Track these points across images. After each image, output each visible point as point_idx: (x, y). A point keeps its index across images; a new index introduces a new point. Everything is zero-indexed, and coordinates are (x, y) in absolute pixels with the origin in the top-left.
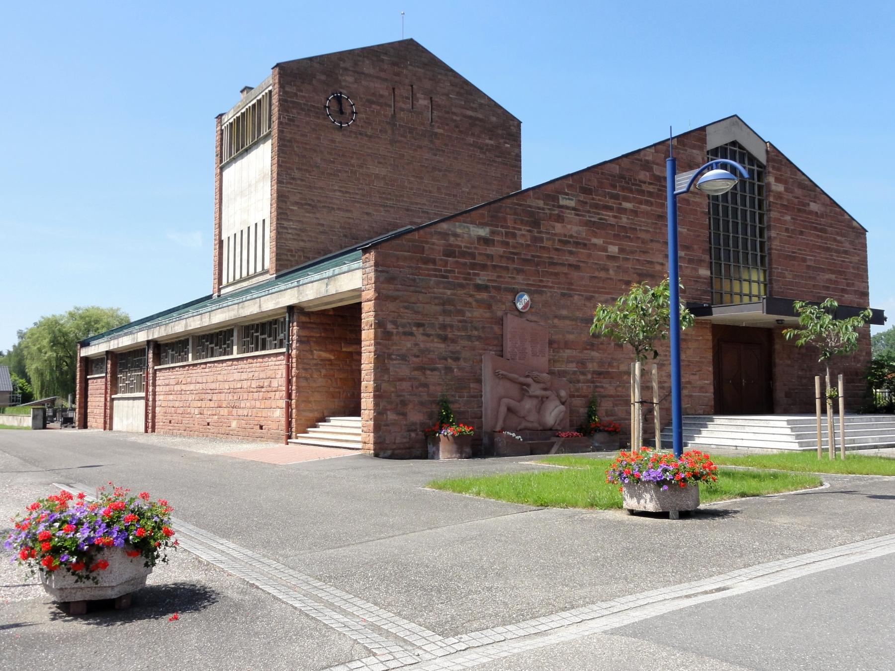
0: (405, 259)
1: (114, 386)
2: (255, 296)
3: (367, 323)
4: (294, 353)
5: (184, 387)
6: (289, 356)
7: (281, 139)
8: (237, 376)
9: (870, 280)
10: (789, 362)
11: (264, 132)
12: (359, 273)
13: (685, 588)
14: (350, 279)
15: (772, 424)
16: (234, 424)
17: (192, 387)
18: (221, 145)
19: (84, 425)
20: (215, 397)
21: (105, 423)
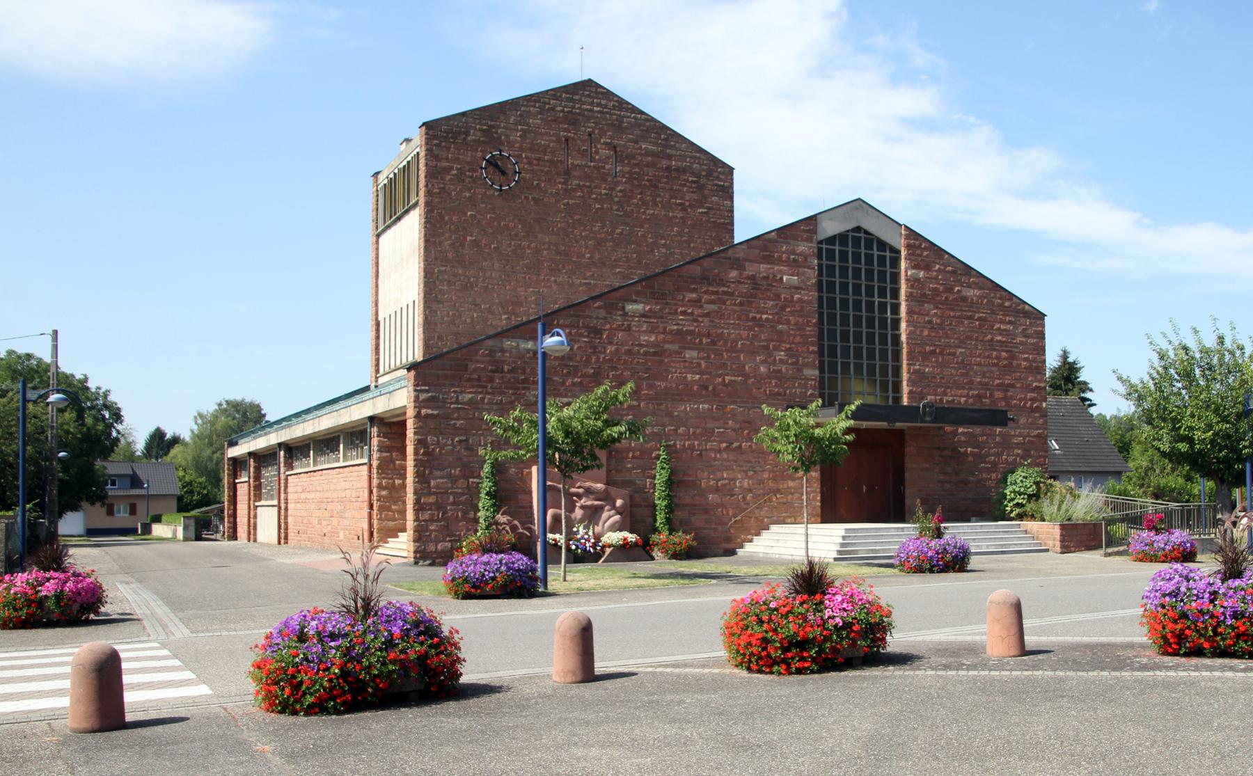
1: (257, 491)
6: (371, 465)
7: (427, 204)
10: (926, 466)
11: (413, 202)
15: (822, 532)
19: (234, 536)
21: (249, 533)
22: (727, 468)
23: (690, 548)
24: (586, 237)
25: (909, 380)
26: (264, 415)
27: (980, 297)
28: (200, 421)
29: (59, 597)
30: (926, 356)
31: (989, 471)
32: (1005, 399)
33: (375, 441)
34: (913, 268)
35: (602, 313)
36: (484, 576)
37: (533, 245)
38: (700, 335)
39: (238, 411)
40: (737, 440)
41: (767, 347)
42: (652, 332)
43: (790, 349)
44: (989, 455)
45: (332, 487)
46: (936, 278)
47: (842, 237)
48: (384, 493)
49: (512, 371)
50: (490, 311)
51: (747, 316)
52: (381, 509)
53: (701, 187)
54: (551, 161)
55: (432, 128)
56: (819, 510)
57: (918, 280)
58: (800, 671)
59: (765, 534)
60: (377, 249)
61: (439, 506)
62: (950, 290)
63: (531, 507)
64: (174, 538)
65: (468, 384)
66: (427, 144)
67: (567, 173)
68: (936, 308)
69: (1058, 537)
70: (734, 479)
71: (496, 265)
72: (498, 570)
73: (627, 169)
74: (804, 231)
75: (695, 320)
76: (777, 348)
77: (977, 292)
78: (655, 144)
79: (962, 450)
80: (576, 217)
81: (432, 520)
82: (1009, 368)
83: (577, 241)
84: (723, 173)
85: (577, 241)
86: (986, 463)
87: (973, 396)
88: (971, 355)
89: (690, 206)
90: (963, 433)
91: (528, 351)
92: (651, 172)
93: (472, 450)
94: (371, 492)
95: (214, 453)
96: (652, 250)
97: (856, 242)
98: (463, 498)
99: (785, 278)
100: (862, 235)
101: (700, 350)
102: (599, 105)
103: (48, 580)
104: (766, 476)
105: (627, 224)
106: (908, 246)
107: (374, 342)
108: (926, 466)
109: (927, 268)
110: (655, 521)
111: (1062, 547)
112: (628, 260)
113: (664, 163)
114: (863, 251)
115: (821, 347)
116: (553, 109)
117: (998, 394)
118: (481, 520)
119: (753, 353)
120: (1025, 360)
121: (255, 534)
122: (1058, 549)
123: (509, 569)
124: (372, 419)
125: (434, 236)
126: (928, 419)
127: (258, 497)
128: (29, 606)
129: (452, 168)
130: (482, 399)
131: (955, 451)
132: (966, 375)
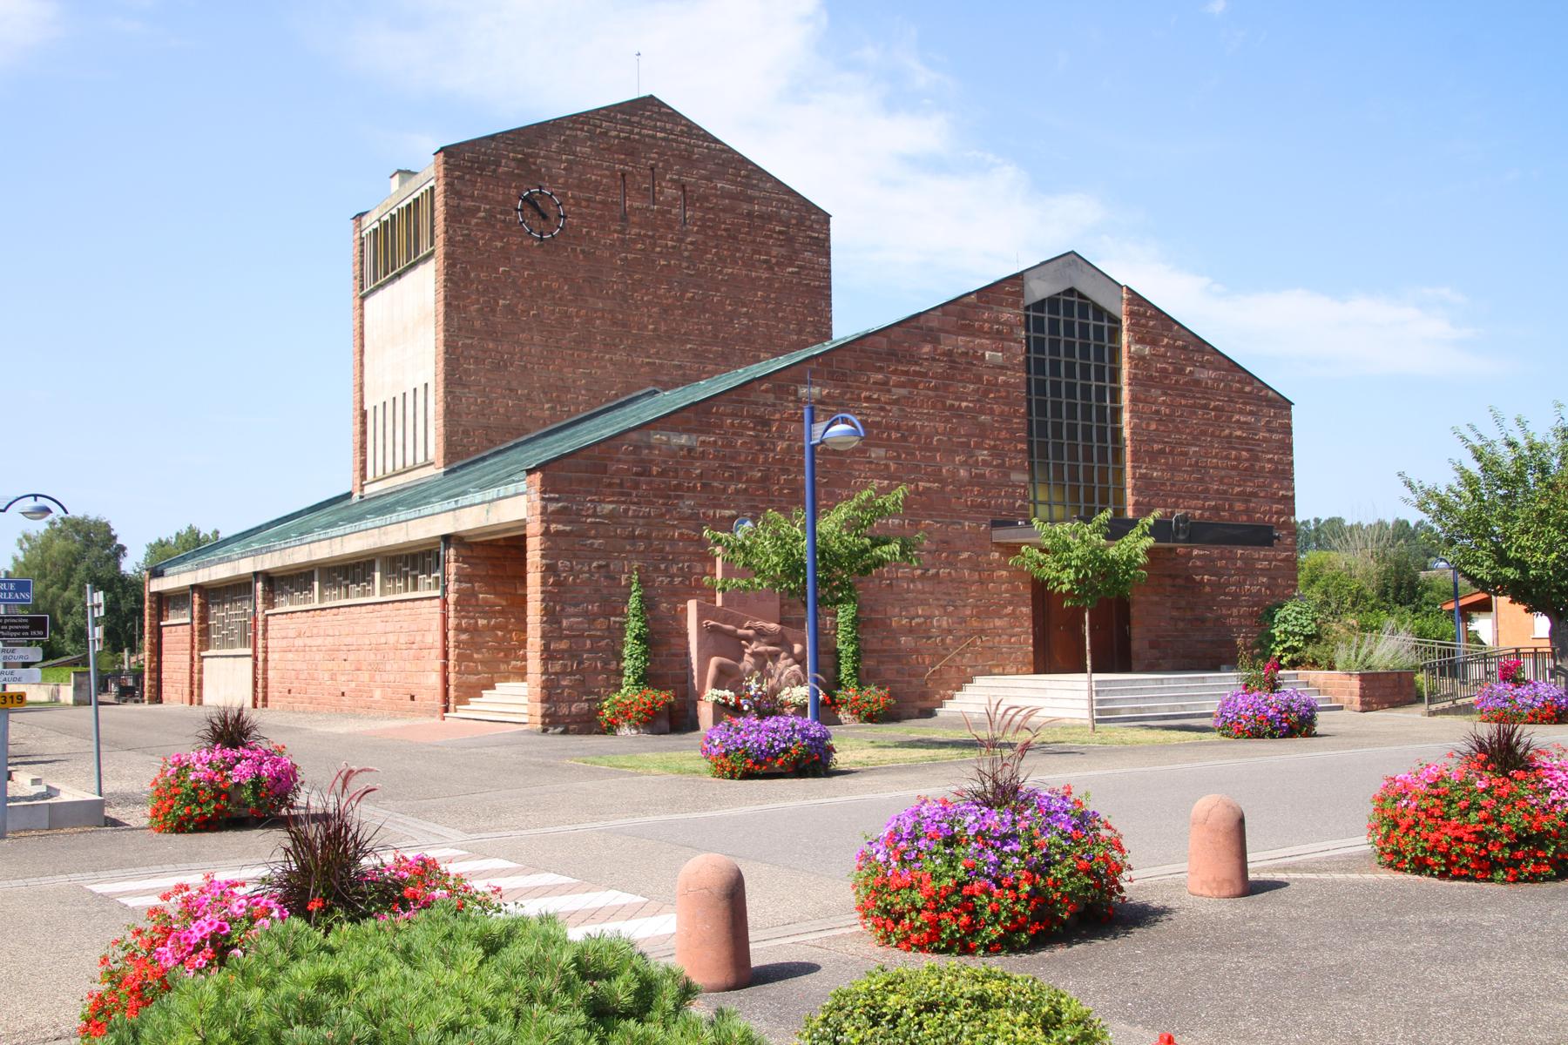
1: (204, 636)
2: (402, 517)
4: (452, 598)
5: (309, 641)
6: (445, 601)
7: (447, 256)
8: (380, 627)
9: (1295, 476)
10: (1156, 599)
14: (513, 504)
16: (378, 694)
17: (319, 641)
18: (362, 263)
19: (157, 698)
20: (351, 657)
21: (192, 693)
22: (924, 603)
23: (888, 707)
24: (649, 302)
25: (1135, 488)
26: (115, 538)
27: (1215, 380)
28: (26, 546)
29: (257, 784)
30: (1154, 457)
31: (1229, 605)
32: (1247, 511)
33: (452, 568)
34: (1137, 342)
35: (771, 398)
36: (772, 747)
37: (583, 312)
38: (888, 428)
39: (78, 532)
40: (933, 566)
41: (967, 445)
43: (995, 447)
44: (1228, 584)
45: (358, 629)
46: (1164, 356)
47: (1052, 303)
48: (464, 637)
49: (662, 474)
50: (529, 399)
51: (944, 404)
52: (460, 658)
53: (790, 240)
54: (603, 203)
55: (450, 154)
56: (1031, 656)
57: (1142, 358)
58: (1533, 878)
59: (969, 688)
60: (362, 315)
61: (573, 654)
62: (1181, 371)
63: (687, 654)
64: (55, 701)
65: (608, 491)
66: (446, 176)
67: (624, 218)
68: (1165, 394)
69: (1357, 690)
70: (930, 617)
71: (537, 338)
72: (790, 739)
74: (1010, 293)
75: (882, 409)
76: (979, 446)
77: (1212, 374)
78: (734, 183)
79: (1198, 578)
80: (636, 276)
81: (564, 673)
82: (1250, 473)
83: (637, 308)
84: (817, 222)
85: (637, 308)
86: (1226, 594)
87: (1210, 508)
88: (1206, 455)
90: (1198, 557)
91: (682, 447)
92: (729, 218)
93: (613, 579)
94: (445, 637)
95: (47, 587)
96: (732, 320)
97: (1069, 306)
98: (603, 643)
99: (987, 354)
100: (1075, 299)
101: (888, 448)
102: (663, 130)
103: (239, 760)
104: (968, 612)
105: (700, 287)
106: (1131, 314)
107: (358, 438)
108: (1156, 599)
109: (1154, 343)
110: (838, 671)
111: (1362, 703)
113: (745, 207)
114: (1076, 319)
115: (1030, 444)
116: (605, 134)
117: (1239, 506)
118: (627, 672)
119: (950, 452)
120: (1270, 461)
121: (200, 695)
122: (1358, 706)
123: (804, 737)
124: (447, 539)
125: (456, 298)
126: (1181, 537)
127: (205, 643)
128: (216, 798)
129: (478, 209)
130: (626, 511)
131: (1189, 579)
132: (1201, 480)
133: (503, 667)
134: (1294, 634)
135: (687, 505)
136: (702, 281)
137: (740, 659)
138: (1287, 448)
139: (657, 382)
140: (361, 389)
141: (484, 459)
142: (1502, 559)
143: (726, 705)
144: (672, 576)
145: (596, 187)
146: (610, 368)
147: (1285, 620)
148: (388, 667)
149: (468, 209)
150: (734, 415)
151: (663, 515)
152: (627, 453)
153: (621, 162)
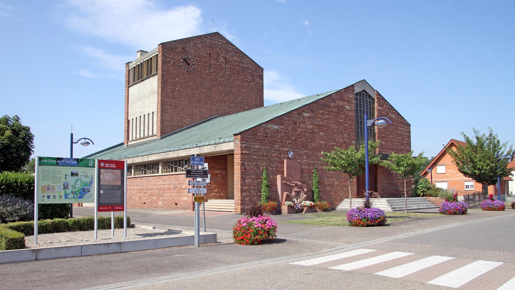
0: (250, 138)
3: (237, 163)
7: (162, 74)
8: (161, 183)
12: (232, 143)
13: (389, 238)
16: (160, 203)
17: (134, 187)
18: (129, 77)
20: (148, 192)
38: (324, 126)
42: (311, 124)
47: (360, 93)
57: (380, 110)
60: (128, 92)
61: (249, 190)
67: (210, 66)
70: (334, 181)
73: (230, 66)
75: (323, 121)
76: (345, 133)
77: (394, 116)
89: (250, 82)
91: (275, 129)
101: (324, 132)
106: (377, 98)
109: (382, 106)
112: (230, 101)
116: (205, 42)
118: (263, 196)
125: (164, 87)
129: (171, 61)
130: (262, 147)
131: (390, 172)
132: (392, 145)
133: (210, 195)
134: (424, 187)
135: (277, 146)
136: (230, 86)
137: (291, 193)
138: (409, 137)
139: (218, 114)
140: (128, 114)
141: (171, 135)
142: (475, 167)
143: (291, 206)
144: (273, 168)
145: (203, 57)
146: (206, 109)
147: (421, 184)
148: (165, 195)
149: (168, 61)
150: (288, 120)
151: (271, 149)
152: (262, 130)
153: (209, 50)
